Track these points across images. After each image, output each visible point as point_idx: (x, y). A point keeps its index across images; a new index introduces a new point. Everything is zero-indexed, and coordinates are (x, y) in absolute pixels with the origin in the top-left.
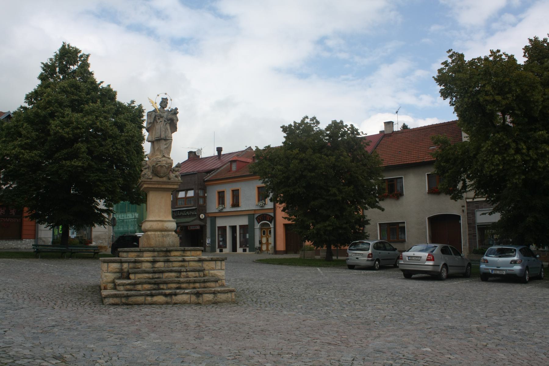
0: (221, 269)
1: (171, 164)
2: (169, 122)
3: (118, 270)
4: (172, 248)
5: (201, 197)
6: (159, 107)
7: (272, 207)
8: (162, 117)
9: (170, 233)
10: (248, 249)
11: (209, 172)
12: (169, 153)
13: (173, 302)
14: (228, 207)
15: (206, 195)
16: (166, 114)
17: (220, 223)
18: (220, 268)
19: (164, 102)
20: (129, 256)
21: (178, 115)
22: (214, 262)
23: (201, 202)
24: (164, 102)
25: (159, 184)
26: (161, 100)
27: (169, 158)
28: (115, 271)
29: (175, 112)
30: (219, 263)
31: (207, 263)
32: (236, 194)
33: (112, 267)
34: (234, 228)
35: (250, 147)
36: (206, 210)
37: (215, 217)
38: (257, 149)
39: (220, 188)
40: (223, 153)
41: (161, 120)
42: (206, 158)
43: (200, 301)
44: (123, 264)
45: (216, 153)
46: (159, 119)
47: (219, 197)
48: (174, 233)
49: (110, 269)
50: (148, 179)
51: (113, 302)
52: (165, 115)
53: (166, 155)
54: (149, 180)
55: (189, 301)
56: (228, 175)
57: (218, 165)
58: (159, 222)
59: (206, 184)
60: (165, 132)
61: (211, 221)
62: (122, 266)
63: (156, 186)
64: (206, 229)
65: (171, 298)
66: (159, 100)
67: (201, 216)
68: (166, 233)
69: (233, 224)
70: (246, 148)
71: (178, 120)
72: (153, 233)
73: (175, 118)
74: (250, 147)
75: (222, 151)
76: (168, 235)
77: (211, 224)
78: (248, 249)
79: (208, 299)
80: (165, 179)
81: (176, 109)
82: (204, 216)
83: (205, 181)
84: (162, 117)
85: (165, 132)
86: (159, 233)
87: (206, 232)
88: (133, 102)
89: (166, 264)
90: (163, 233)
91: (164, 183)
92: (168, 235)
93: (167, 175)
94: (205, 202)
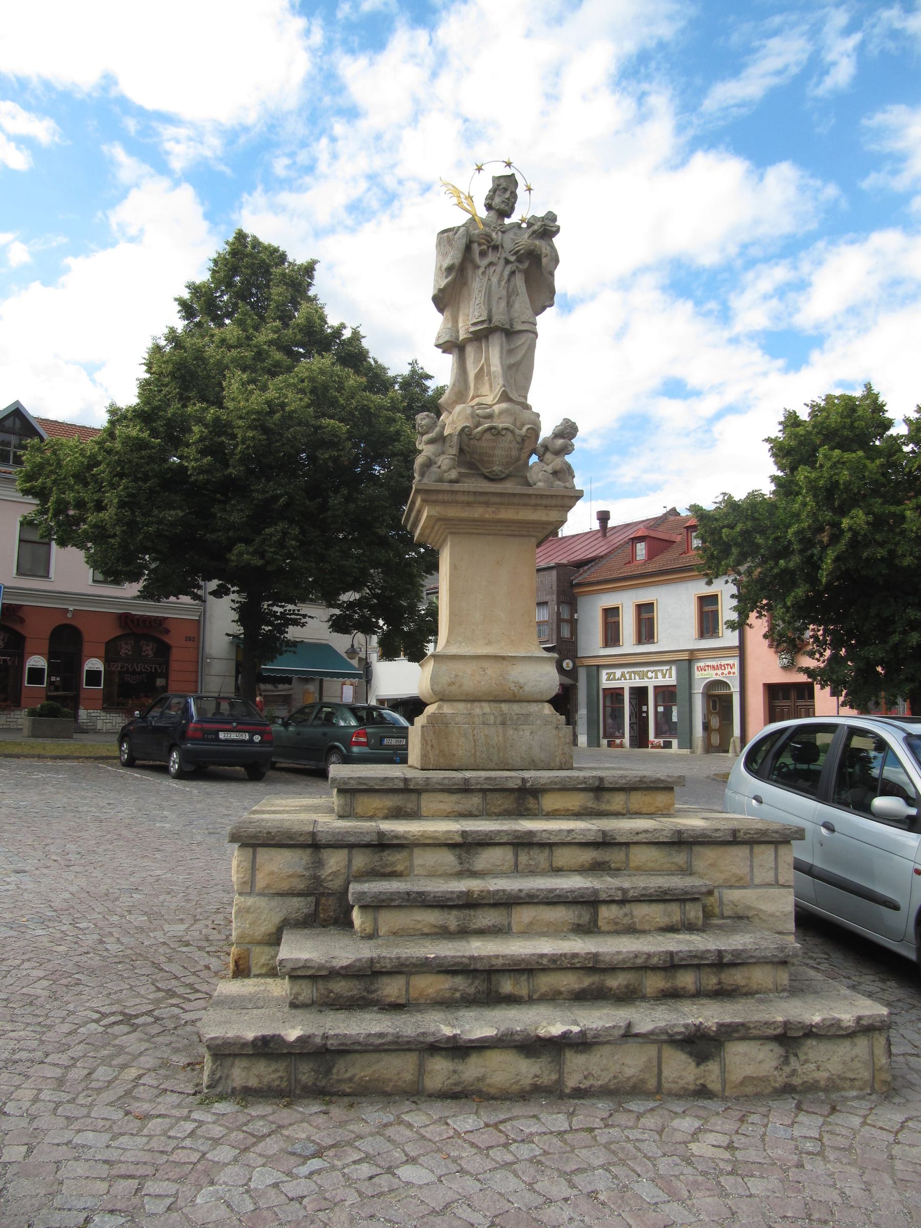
0: (777, 884)
1: (535, 430)
2: (526, 265)
3: (301, 886)
4: (545, 776)
5: (565, 621)
6: (482, 213)
7: (736, 643)
8: (495, 248)
9: (534, 708)
10: (675, 742)
11: (580, 565)
12: (526, 388)
13: (572, 1082)
14: (628, 643)
15: (576, 616)
16: (510, 235)
17: (606, 681)
18: (769, 877)
19: (504, 192)
20: (359, 810)
21: (556, 240)
22: (741, 852)
23: (566, 632)
24: (504, 192)
25: (487, 504)
26: (490, 185)
27: (528, 407)
28: (285, 886)
29: (546, 229)
30: (765, 854)
31: (709, 854)
32: (645, 611)
33: (273, 867)
34: (640, 694)
35: (674, 510)
36: (575, 650)
37: (598, 666)
38: (696, 509)
39: (608, 600)
40: (611, 524)
41: (491, 257)
42: (574, 536)
43: (713, 1080)
44: (325, 854)
45: (596, 525)
46: (483, 254)
47: (606, 624)
48: (548, 709)
49: (261, 881)
50: (441, 480)
51: (253, 1083)
52: (508, 242)
53: (514, 395)
54: (446, 486)
55: (652, 1084)
56: (628, 571)
57: (600, 549)
58: (485, 664)
59: (576, 591)
60: (509, 305)
61: (589, 676)
62: (319, 864)
63: (477, 512)
64: (576, 694)
65: (558, 1062)
66: (481, 188)
67: (565, 665)
68: (516, 708)
69: (638, 682)
70: (665, 511)
71: (557, 261)
72: (461, 706)
73: (545, 249)
74: (674, 510)
75: (609, 519)
76: (525, 718)
77: (589, 682)
78: (675, 742)
79: (749, 1071)
80: (509, 486)
81: (551, 217)
82: (571, 665)
83: (573, 586)
84: (495, 248)
85: (509, 305)
86: (486, 707)
87: (576, 699)
88: (393, 217)
89: (523, 858)
90: (504, 707)
91: (507, 499)
92: (525, 718)
93: (518, 471)
94: (574, 632)
